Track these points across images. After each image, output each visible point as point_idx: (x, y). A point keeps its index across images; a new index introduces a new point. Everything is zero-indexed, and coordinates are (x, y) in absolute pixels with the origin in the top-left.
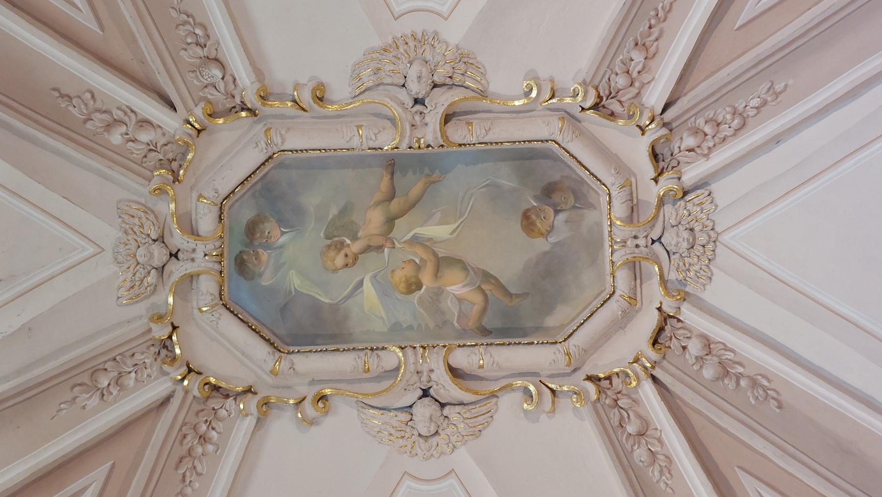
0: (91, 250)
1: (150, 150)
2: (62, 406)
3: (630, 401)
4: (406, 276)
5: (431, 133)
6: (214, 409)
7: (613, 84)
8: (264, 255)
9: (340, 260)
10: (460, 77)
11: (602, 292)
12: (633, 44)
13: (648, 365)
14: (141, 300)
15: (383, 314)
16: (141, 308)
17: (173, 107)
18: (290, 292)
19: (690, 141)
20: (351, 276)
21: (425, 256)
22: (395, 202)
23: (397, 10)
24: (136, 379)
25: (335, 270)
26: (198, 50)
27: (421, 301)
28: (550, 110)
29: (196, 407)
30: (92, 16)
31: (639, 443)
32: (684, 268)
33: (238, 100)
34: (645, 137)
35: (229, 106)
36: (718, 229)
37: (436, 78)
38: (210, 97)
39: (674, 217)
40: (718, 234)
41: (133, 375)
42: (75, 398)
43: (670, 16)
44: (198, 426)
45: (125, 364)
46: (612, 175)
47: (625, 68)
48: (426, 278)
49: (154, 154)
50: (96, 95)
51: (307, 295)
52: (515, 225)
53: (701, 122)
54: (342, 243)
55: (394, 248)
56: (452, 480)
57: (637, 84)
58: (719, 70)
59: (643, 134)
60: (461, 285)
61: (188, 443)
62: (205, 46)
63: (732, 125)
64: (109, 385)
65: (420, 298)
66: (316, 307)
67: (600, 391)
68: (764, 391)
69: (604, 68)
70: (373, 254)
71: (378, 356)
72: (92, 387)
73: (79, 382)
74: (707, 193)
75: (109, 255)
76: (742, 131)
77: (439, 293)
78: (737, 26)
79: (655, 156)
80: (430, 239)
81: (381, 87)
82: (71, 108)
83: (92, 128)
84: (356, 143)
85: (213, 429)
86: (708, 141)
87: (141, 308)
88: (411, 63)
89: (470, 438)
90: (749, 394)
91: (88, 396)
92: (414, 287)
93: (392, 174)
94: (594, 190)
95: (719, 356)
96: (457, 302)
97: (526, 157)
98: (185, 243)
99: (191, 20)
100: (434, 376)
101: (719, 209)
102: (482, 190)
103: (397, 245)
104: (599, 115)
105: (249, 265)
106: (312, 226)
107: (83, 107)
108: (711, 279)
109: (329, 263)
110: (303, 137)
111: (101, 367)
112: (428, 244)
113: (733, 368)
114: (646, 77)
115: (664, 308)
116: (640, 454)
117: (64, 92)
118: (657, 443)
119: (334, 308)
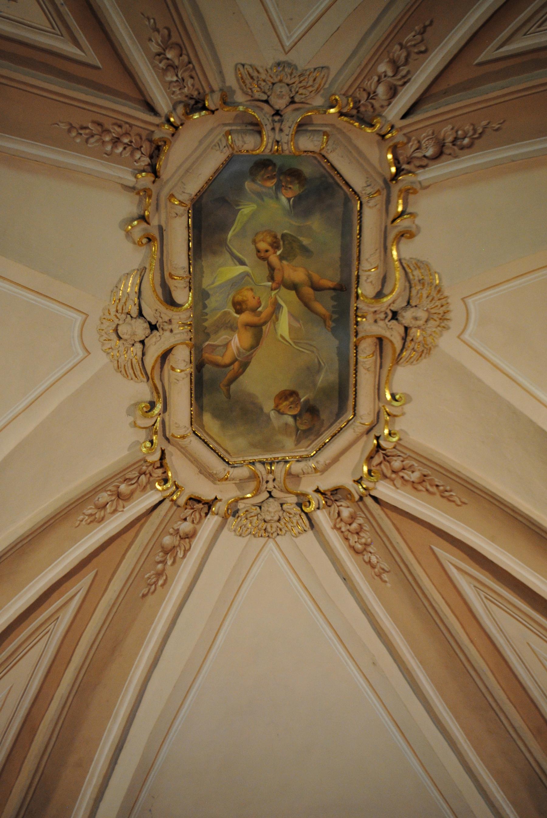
0: (287, 44)
1: (369, 94)
2: (152, 21)
3: (144, 484)
4: (247, 300)
5: (368, 326)
6: (141, 147)
7: (395, 458)
8: (271, 184)
9: (263, 246)
10: (411, 347)
11: (229, 454)
12: (425, 473)
13: (175, 497)
14: (239, 84)
15: (217, 283)
16: (231, 81)
17: (404, 117)
18: (238, 205)
19: (346, 513)
20: (250, 257)
21: (263, 315)
22: (311, 291)
23: (470, 301)
24: (171, 82)
25: (254, 242)
26: (450, 139)
27: (226, 314)
28: (379, 412)
29: (144, 134)
30: (489, 58)
31: (112, 495)
32: (249, 516)
33: (405, 166)
34: (351, 483)
35: (401, 158)
36: (278, 539)
37: (413, 330)
38: (410, 144)
39: (289, 507)
40: (274, 539)
41: (175, 79)
42: (158, 31)
43: (445, 501)
44: (128, 136)
45: (184, 71)
46: (325, 462)
47: (406, 467)
48: (246, 317)
49: (365, 96)
50: (421, 55)
51: (234, 220)
52: (285, 386)
53: (361, 521)
54: (278, 248)
55: (272, 290)
56: (81, 353)
57: (394, 476)
58: (400, 533)
59: (354, 481)
60: (239, 345)
61: (114, 129)
62: (454, 145)
63: (357, 544)
64: (168, 59)
65: (229, 313)
66: (225, 227)
67: (153, 464)
68: (154, 582)
69: (409, 453)
70: (266, 272)
71: (185, 288)
72: (166, 45)
73: (172, 34)
74: (306, 529)
75: (282, 58)
76: (353, 552)
77: (232, 327)
78: (433, 547)
79: (335, 491)
80: (277, 319)
81: (407, 284)
82: (413, 34)
83: (394, 49)
84: (365, 265)
85: (125, 148)
86: (345, 526)
87: (231, 81)
88: (427, 310)
89: (116, 365)
90: (152, 572)
91: (160, 43)
92: (238, 307)
93: (334, 289)
94: (311, 444)
95: (179, 546)
96: (224, 343)
97: (341, 395)
98: (288, 124)
99: (476, 136)
100: (167, 333)
101: (294, 539)
102: (316, 360)
103: (274, 293)
104: (372, 451)
105: (262, 172)
106: (294, 223)
107: (413, 43)
108: (240, 535)
109: (262, 237)
110: (371, 219)
111: (184, 52)
112: (274, 317)
113: (170, 557)
114: (398, 482)
115: (218, 504)
116: (104, 497)
117: (429, 29)
118: (113, 508)
119: (223, 243)
